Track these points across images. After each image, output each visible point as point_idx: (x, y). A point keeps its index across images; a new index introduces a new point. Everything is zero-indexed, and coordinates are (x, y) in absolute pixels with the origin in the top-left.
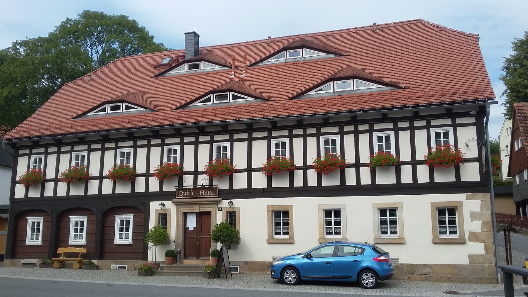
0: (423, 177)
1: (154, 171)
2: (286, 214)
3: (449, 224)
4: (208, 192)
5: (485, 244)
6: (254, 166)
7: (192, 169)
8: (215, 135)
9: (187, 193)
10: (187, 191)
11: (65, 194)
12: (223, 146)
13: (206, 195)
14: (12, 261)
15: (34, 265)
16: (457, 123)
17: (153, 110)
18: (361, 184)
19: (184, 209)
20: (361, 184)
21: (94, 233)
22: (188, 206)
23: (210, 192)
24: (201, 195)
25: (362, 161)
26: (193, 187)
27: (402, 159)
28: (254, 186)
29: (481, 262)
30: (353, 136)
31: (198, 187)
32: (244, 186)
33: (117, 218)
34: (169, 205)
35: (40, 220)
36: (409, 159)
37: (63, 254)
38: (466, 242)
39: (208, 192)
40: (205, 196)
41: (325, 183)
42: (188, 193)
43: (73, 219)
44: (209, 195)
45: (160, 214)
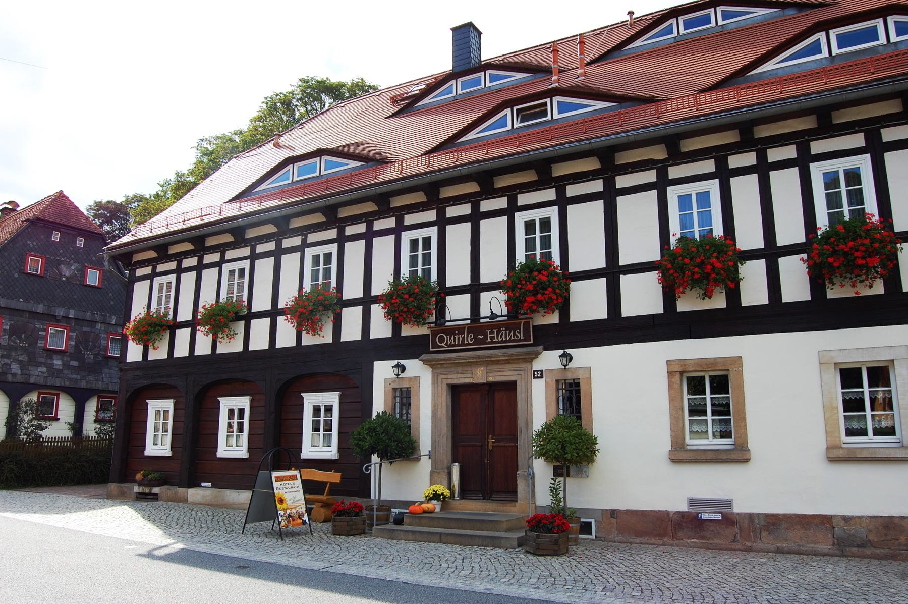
0: (381, 328)
1: (826, 229)
2: (721, 384)
4: (506, 334)
7: (466, 280)
8: (520, 193)
9: (455, 338)
10: (457, 332)
11: (208, 351)
12: (422, 238)
13: (502, 342)
14: (121, 487)
15: (155, 497)
16: (885, 140)
17: (381, 162)
18: (331, 342)
19: (449, 376)
20: (331, 342)
22: (460, 369)
23: (512, 333)
25: (782, 240)
26: (469, 322)
28: (625, 313)
30: (754, 178)
31: (447, 324)
32: (601, 313)
33: (224, 405)
34: (414, 367)
35: (244, 402)
36: (759, 244)
37: (329, 484)
38: (750, 459)
39: (508, 332)
40: (499, 342)
41: (684, 305)
42: (459, 338)
43: (310, 400)
44: (510, 341)
45: (395, 389)
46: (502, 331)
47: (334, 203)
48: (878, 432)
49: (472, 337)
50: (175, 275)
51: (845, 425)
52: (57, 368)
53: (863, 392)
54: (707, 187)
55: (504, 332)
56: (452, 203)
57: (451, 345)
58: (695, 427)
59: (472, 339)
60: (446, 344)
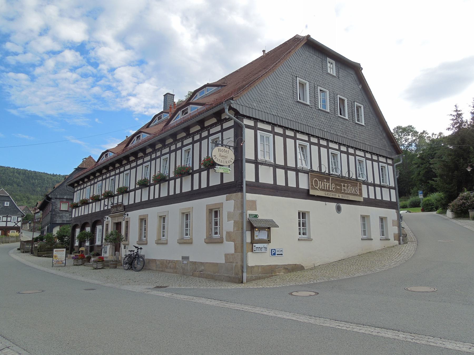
5: (235, 243)
6: (6, 222)
9: (324, 184)
21: (33, 233)
29: (231, 261)
39: (352, 188)
42: (326, 184)
47: (201, 119)
50: (191, 145)
56: (225, 121)
57: (114, 211)
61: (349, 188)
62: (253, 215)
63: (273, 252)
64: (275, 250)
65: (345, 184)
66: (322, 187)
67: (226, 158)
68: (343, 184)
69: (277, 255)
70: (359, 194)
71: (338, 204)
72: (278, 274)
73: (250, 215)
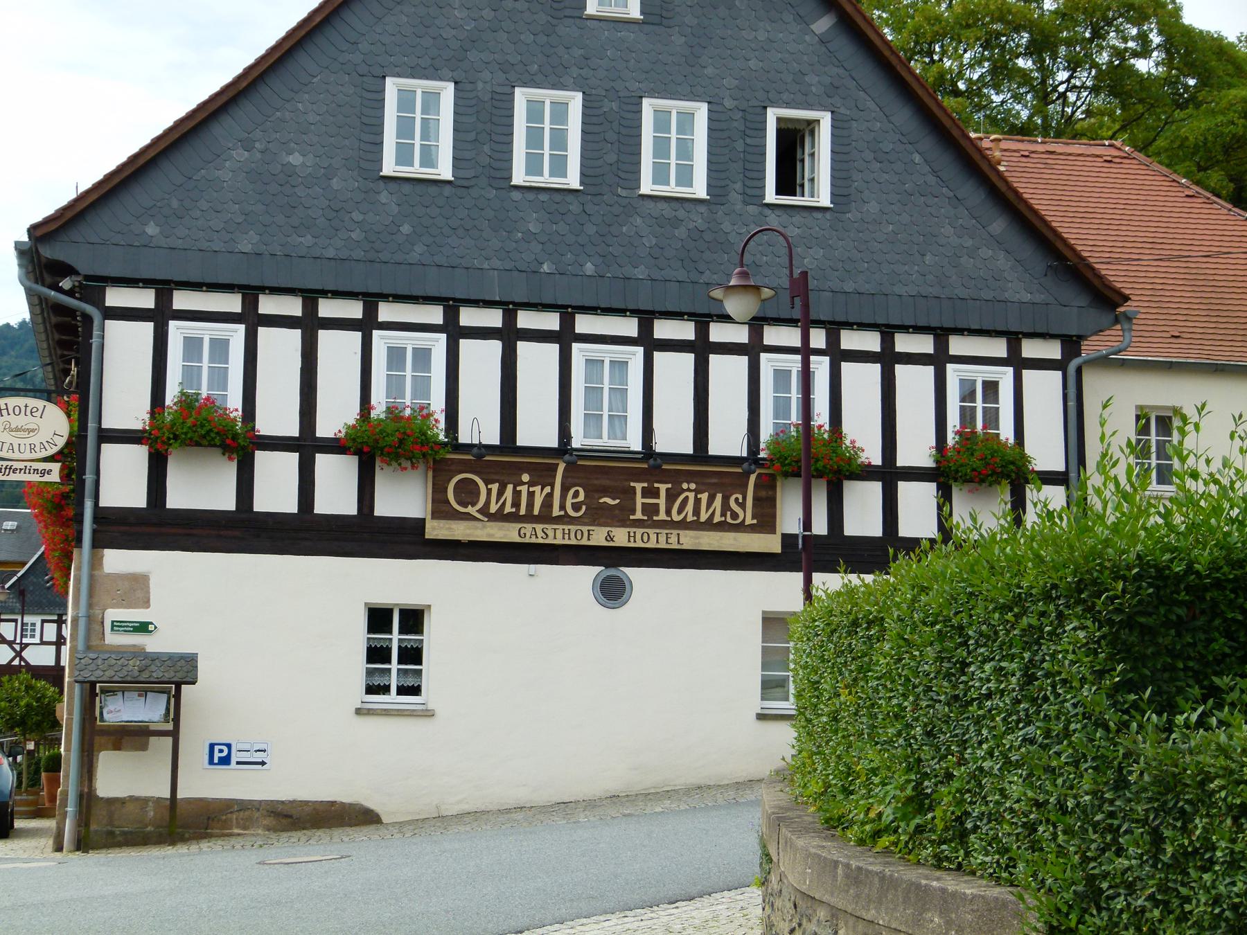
3: (401, 632)
4: (698, 502)
9: (517, 494)
24: (639, 515)
27: (265, 426)
39: (704, 497)
42: (531, 495)
46: (684, 491)
48: (402, 691)
49: (581, 497)
51: (366, 681)
52: (76, 428)
53: (391, 639)
54: (404, 342)
55: (691, 496)
58: (410, 679)
59: (581, 503)
60: (484, 511)
61: (687, 498)
62: (131, 625)
63: (217, 755)
64: (229, 746)
65: (656, 485)
66: (504, 504)
67: (31, 434)
68: (645, 485)
69: (238, 763)
70: (749, 521)
71: (612, 572)
72: (236, 831)
73: (115, 624)
